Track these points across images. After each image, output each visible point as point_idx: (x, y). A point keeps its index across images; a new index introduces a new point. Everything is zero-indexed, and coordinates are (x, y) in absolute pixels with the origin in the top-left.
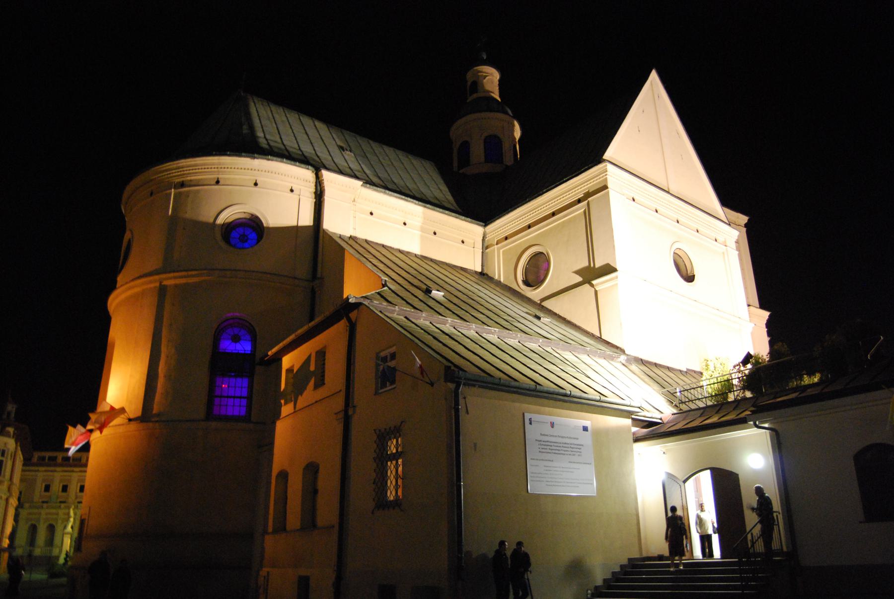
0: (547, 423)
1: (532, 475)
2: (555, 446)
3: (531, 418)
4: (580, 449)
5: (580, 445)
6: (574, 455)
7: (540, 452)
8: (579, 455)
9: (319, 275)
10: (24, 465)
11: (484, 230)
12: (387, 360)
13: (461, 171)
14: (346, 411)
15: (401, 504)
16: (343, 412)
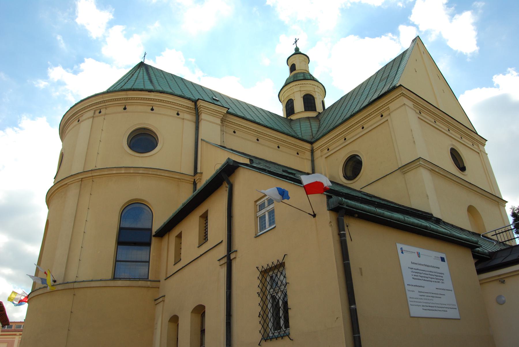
0: (415, 253)
1: (411, 300)
2: (424, 274)
3: (402, 248)
4: (442, 277)
5: (442, 274)
6: (438, 282)
7: (413, 278)
8: (442, 283)
9: (199, 171)
10: (14, 341)
11: (311, 146)
12: (265, 205)
13: (289, 118)
14: (228, 256)
15: (289, 334)
16: (226, 264)
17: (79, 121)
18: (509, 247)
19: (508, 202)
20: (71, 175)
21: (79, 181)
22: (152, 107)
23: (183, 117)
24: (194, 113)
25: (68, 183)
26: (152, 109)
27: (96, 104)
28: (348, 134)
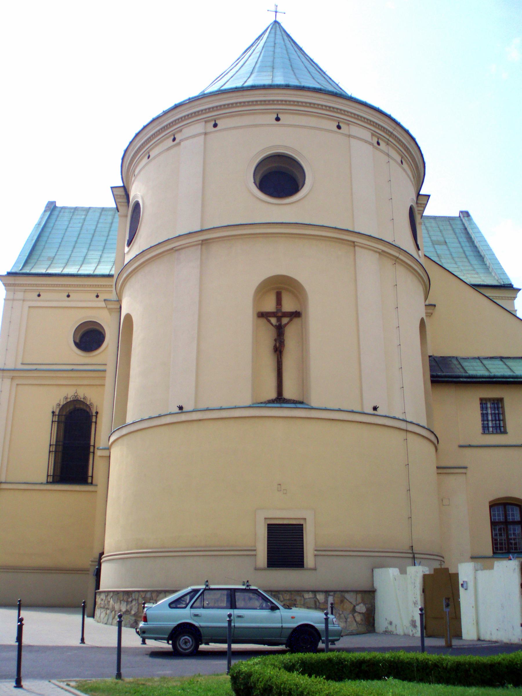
17: (149, 157)
18: (281, 596)
19: (520, 290)
20: (177, 235)
21: (198, 244)
22: (277, 115)
23: (348, 134)
24: (123, 202)
25: (174, 247)
26: (278, 119)
27: (158, 133)
28: (46, 291)
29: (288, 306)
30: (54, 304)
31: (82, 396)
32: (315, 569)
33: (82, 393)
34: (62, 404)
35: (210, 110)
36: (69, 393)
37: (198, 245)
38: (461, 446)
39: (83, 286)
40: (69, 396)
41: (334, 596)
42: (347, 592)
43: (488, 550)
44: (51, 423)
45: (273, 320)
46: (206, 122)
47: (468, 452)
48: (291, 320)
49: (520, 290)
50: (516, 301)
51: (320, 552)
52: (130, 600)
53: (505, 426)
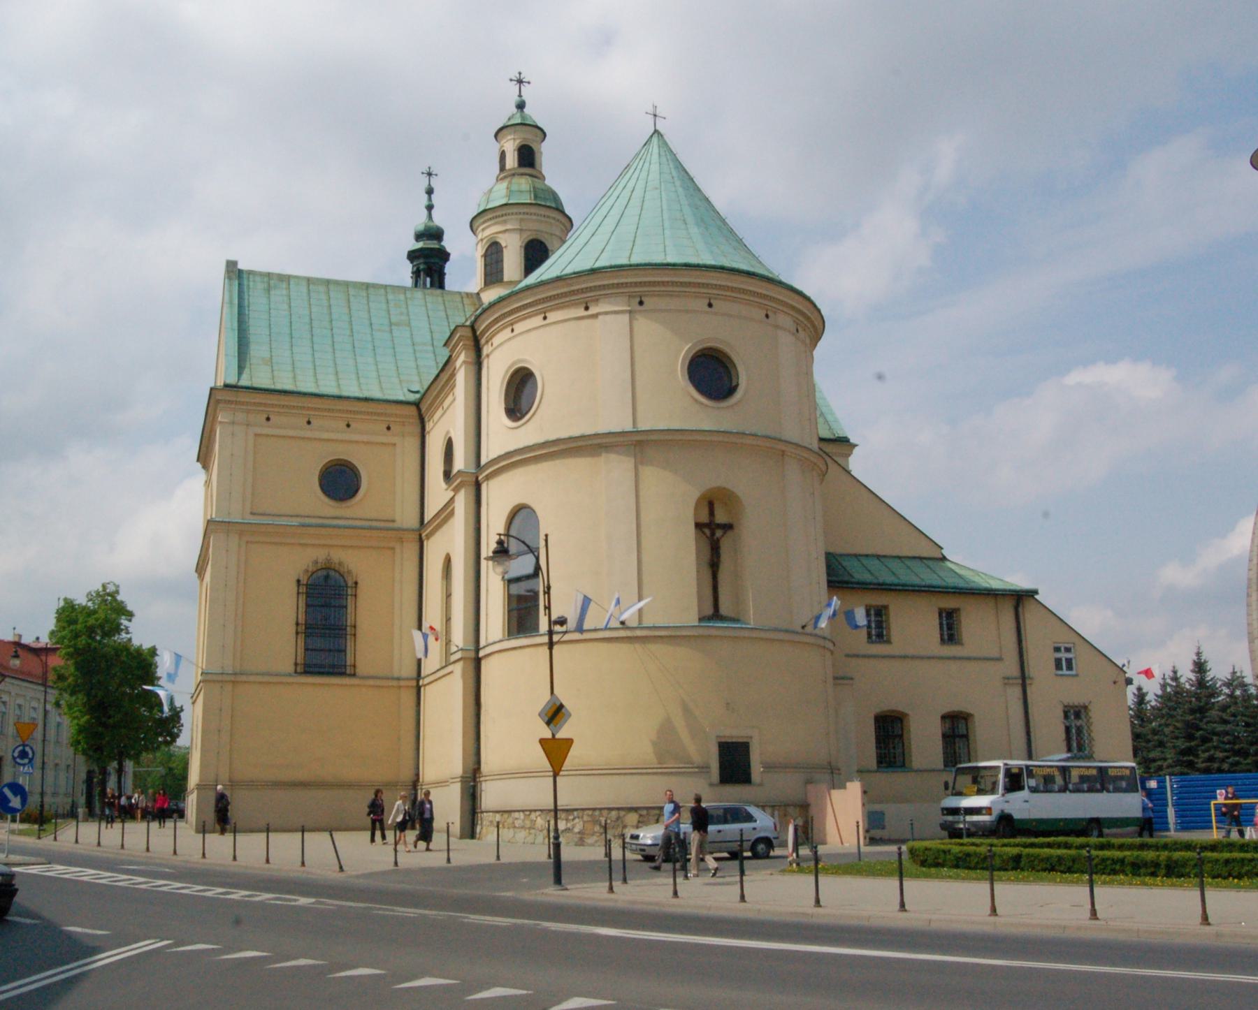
19: (857, 445)
26: (710, 305)
29: (721, 518)
30: (291, 433)
31: (337, 561)
32: (761, 785)
33: (337, 556)
34: (310, 569)
35: (636, 284)
36: (321, 555)
37: (632, 444)
38: (847, 656)
39: (329, 410)
40: (320, 560)
41: (779, 810)
42: (788, 805)
43: (872, 763)
44: (295, 595)
45: (707, 531)
46: (629, 296)
47: (854, 661)
48: (725, 533)
49: (857, 445)
50: (851, 459)
51: (769, 767)
52: (571, 817)
53: (888, 635)
